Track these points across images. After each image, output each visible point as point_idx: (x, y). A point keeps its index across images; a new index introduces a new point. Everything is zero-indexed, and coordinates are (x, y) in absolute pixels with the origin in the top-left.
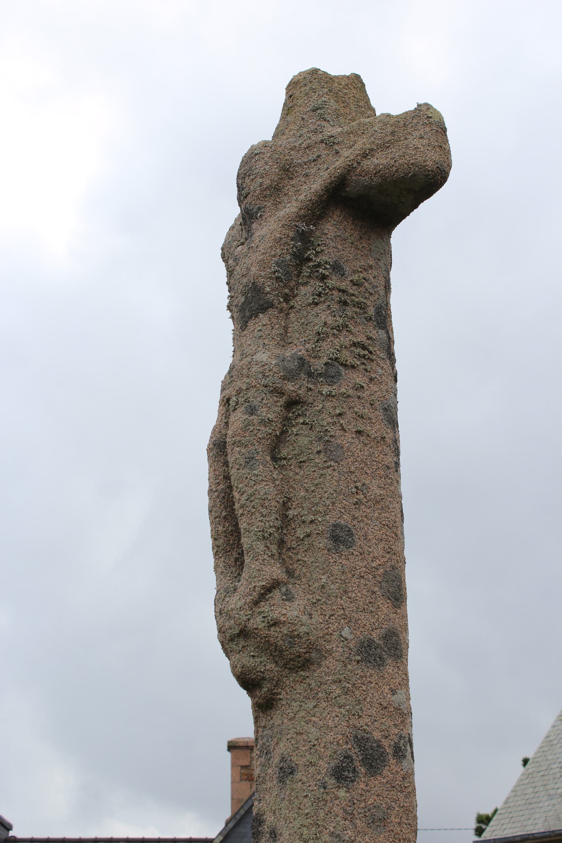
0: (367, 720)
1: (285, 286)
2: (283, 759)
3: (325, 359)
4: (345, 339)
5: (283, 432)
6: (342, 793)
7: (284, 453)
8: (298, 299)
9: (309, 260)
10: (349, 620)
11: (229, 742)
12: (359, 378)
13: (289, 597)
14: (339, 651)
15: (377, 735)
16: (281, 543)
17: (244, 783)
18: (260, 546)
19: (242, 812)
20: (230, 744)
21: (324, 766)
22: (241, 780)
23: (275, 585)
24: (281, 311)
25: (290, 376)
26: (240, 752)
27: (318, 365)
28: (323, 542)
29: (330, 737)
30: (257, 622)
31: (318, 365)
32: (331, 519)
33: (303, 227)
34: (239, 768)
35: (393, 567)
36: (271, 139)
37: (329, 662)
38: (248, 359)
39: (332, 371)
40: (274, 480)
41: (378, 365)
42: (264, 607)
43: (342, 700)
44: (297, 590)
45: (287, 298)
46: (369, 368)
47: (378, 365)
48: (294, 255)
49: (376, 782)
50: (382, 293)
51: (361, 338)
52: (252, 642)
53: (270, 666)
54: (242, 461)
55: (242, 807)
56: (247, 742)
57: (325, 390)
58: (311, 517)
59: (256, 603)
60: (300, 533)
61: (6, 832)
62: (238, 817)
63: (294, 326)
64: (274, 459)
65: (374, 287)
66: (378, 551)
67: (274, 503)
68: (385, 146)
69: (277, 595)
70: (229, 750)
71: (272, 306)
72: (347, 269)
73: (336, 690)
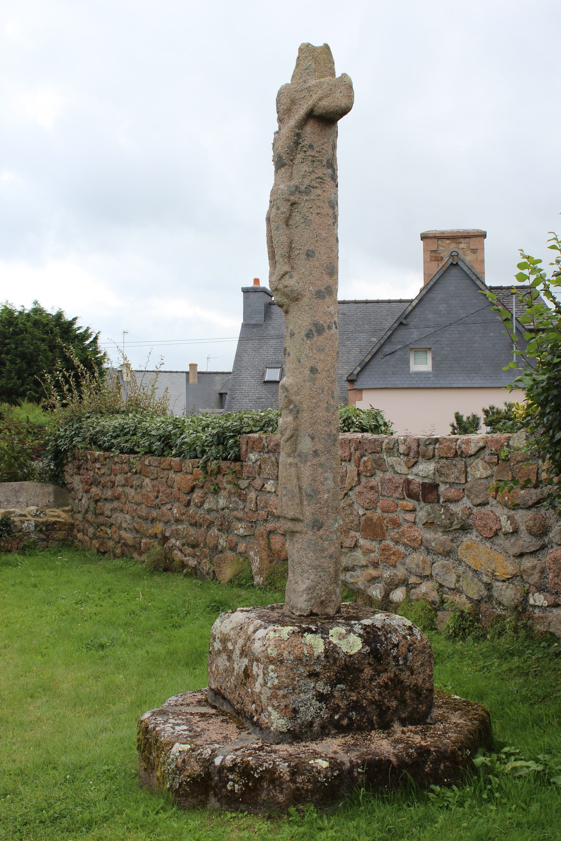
0: (318, 317)
1: (291, 156)
2: (291, 331)
3: (305, 186)
4: (313, 176)
5: (290, 215)
6: (308, 342)
7: (290, 223)
8: (296, 160)
9: (300, 143)
10: (312, 284)
11: (421, 234)
12: (319, 192)
13: (291, 277)
14: (308, 295)
15: (321, 322)
16: (289, 257)
17: (433, 262)
18: (281, 260)
19: (432, 283)
20: (422, 236)
21: (303, 333)
22: (431, 261)
23: (286, 273)
24: (290, 166)
25: (292, 194)
26: (430, 241)
27: (303, 188)
28: (304, 257)
29: (305, 324)
30: (280, 286)
31: (303, 188)
32: (306, 248)
33: (297, 131)
34: (429, 252)
35: (330, 263)
36: (290, 82)
37: (305, 299)
38: (277, 187)
39: (307, 191)
40: (286, 234)
41: (327, 184)
42: (283, 281)
43: (309, 312)
44: (294, 274)
45: (292, 160)
46: (323, 186)
47: (327, 184)
48: (294, 143)
49: (321, 338)
50: (330, 152)
51: (320, 175)
52: (279, 292)
53: (286, 300)
54: (275, 228)
55: (432, 280)
56: (435, 234)
57: (305, 198)
58: (300, 247)
59: (280, 280)
60: (296, 253)
61: (270, 298)
62: (429, 287)
63: (295, 172)
64: (287, 225)
65: (326, 151)
66: (324, 257)
67: (286, 243)
68: (327, 96)
69: (287, 276)
70: (421, 240)
71: (286, 164)
72: (315, 145)
73: (307, 308)
